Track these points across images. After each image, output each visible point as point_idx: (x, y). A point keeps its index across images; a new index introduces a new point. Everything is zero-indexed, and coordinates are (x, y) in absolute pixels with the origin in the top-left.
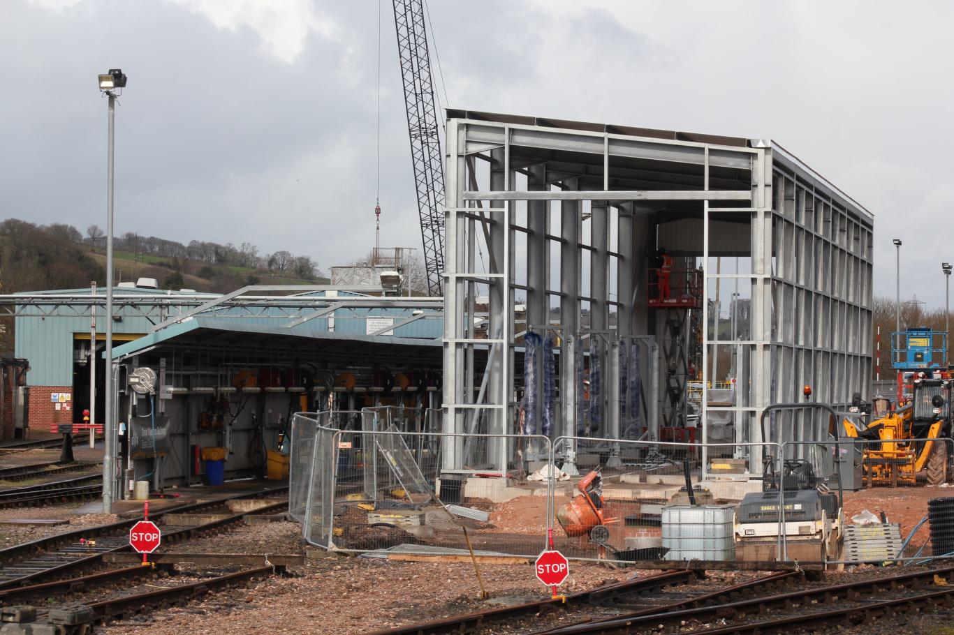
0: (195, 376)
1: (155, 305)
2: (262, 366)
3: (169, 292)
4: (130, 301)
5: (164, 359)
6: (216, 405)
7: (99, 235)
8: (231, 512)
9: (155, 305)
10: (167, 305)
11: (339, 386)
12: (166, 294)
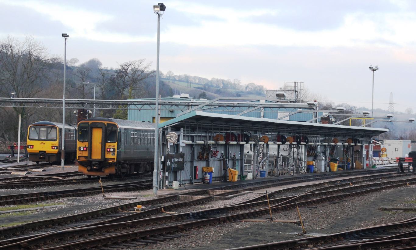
0: (364, 141)
1: (186, 105)
2: (227, 132)
5: (183, 129)
6: (205, 149)
7: (172, 75)
8: (209, 195)
9: (186, 105)
10: (191, 105)
11: (262, 142)
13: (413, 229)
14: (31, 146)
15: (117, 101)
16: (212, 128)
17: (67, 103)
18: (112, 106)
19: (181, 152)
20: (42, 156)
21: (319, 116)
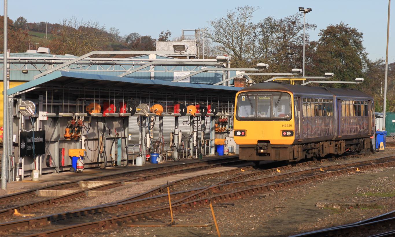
3: (54, 55)
4: (30, 61)
5: (42, 96)
12: (52, 57)
14: (241, 131)
20: (262, 151)
21: (230, 77)
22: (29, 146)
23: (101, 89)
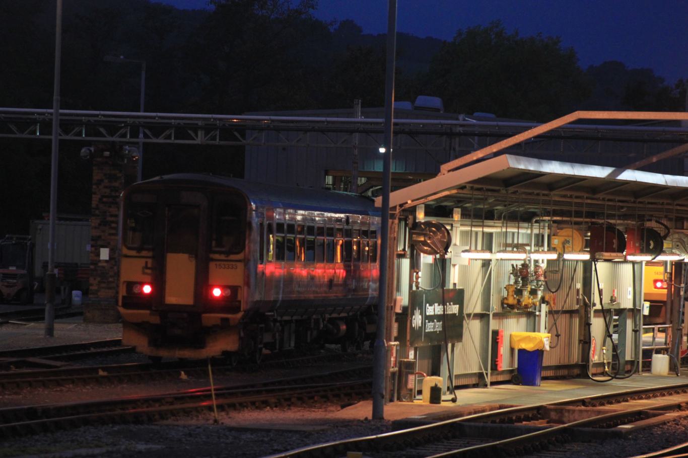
2: (593, 223)
13: (681, 398)
15: (220, 119)
16: (582, 212)
17: (402, 132)
18: (206, 135)
19: (455, 284)
22: (429, 322)
23: (587, 198)
